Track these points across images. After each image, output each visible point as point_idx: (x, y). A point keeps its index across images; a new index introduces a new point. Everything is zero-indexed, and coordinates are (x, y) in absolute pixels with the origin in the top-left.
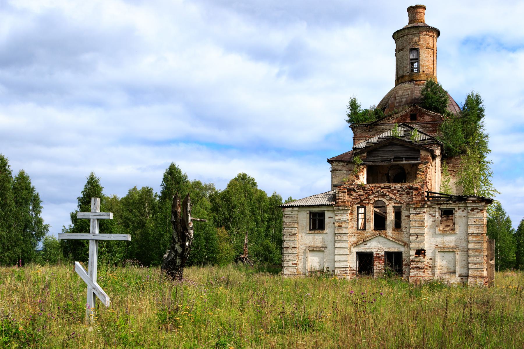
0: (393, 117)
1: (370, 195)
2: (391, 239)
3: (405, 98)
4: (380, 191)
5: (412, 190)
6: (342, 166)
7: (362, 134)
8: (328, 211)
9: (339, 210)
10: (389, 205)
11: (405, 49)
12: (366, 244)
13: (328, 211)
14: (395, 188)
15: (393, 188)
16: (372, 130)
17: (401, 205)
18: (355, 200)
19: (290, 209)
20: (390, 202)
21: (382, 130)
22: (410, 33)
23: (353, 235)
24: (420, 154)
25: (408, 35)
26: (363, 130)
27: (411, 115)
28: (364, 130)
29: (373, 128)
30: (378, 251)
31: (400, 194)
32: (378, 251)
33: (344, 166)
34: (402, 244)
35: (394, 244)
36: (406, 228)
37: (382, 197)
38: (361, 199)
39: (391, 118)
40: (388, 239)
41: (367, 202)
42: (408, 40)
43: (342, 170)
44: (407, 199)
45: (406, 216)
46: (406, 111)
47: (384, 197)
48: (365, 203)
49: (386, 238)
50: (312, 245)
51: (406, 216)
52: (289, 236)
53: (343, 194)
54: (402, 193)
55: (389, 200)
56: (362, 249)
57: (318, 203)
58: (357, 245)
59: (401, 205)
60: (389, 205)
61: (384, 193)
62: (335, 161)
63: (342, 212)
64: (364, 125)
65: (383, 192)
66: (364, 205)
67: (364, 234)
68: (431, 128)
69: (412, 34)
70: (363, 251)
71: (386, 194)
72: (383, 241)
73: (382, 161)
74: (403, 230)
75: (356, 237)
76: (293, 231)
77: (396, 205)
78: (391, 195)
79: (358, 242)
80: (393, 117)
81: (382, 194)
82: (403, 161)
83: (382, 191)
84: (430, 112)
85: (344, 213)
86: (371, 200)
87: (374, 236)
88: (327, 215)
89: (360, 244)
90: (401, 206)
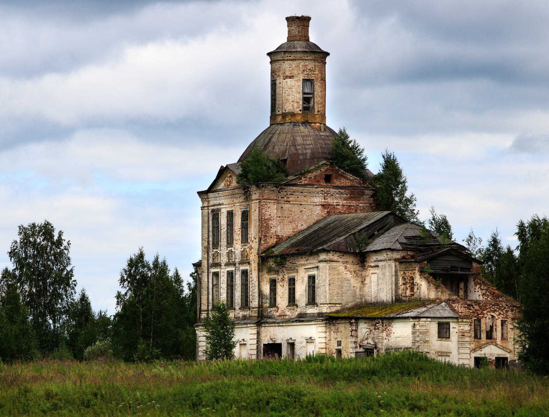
0: (306, 177)
1: (484, 311)
2: (500, 347)
3: (309, 149)
4: (492, 307)
5: (515, 308)
6: (338, 256)
7: (270, 195)
8: (452, 322)
9: (463, 322)
10: (498, 319)
11: (297, 79)
12: (481, 351)
13: (452, 322)
14: (502, 305)
15: (501, 305)
16: (282, 191)
17: (507, 319)
18: (473, 314)
19: (425, 319)
20: (499, 316)
21: (293, 192)
22: (304, 58)
23: (472, 342)
24: (472, 266)
25: (302, 60)
26: (271, 191)
27: (326, 175)
28: (273, 191)
29: (284, 189)
30: (491, 356)
31: (506, 311)
32: (491, 356)
33: (340, 257)
34: (508, 351)
35: (502, 351)
36: (511, 338)
37: (493, 312)
38: (477, 313)
39: (304, 178)
40: (498, 347)
41: (482, 316)
42: (300, 66)
43: (338, 261)
44: (511, 315)
45: (511, 329)
46: (321, 171)
47: (494, 313)
48: (480, 317)
49: (496, 346)
50: (440, 350)
51: (511, 329)
52: (423, 343)
53: (464, 309)
54: (508, 310)
55: (498, 315)
56: (478, 354)
57: (445, 316)
58: (475, 351)
59: (507, 319)
60: (498, 319)
61: (495, 309)
62: (332, 251)
63: (465, 323)
64: (275, 185)
65: (494, 309)
66: (480, 318)
67: (480, 342)
68: (349, 195)
69: (306, 60)
70: (480, 356)
71: (496, 310)
72: (494, 348)
73: (442, 270)
74: (509, 340)
75: (474, 344)
76: (426, 338)
77: (503, 319)
78: (500, 311)
79: (476, 349)
80: (306, 177)
81: (493, 310)
82: (458, 271)
83: (493, 307)
84: (349, 174)
85: (466, 324)
86: (485, 314)
87: (487, 344)
88: (452, 325)
89: (478, 350)
90: (507, 320)
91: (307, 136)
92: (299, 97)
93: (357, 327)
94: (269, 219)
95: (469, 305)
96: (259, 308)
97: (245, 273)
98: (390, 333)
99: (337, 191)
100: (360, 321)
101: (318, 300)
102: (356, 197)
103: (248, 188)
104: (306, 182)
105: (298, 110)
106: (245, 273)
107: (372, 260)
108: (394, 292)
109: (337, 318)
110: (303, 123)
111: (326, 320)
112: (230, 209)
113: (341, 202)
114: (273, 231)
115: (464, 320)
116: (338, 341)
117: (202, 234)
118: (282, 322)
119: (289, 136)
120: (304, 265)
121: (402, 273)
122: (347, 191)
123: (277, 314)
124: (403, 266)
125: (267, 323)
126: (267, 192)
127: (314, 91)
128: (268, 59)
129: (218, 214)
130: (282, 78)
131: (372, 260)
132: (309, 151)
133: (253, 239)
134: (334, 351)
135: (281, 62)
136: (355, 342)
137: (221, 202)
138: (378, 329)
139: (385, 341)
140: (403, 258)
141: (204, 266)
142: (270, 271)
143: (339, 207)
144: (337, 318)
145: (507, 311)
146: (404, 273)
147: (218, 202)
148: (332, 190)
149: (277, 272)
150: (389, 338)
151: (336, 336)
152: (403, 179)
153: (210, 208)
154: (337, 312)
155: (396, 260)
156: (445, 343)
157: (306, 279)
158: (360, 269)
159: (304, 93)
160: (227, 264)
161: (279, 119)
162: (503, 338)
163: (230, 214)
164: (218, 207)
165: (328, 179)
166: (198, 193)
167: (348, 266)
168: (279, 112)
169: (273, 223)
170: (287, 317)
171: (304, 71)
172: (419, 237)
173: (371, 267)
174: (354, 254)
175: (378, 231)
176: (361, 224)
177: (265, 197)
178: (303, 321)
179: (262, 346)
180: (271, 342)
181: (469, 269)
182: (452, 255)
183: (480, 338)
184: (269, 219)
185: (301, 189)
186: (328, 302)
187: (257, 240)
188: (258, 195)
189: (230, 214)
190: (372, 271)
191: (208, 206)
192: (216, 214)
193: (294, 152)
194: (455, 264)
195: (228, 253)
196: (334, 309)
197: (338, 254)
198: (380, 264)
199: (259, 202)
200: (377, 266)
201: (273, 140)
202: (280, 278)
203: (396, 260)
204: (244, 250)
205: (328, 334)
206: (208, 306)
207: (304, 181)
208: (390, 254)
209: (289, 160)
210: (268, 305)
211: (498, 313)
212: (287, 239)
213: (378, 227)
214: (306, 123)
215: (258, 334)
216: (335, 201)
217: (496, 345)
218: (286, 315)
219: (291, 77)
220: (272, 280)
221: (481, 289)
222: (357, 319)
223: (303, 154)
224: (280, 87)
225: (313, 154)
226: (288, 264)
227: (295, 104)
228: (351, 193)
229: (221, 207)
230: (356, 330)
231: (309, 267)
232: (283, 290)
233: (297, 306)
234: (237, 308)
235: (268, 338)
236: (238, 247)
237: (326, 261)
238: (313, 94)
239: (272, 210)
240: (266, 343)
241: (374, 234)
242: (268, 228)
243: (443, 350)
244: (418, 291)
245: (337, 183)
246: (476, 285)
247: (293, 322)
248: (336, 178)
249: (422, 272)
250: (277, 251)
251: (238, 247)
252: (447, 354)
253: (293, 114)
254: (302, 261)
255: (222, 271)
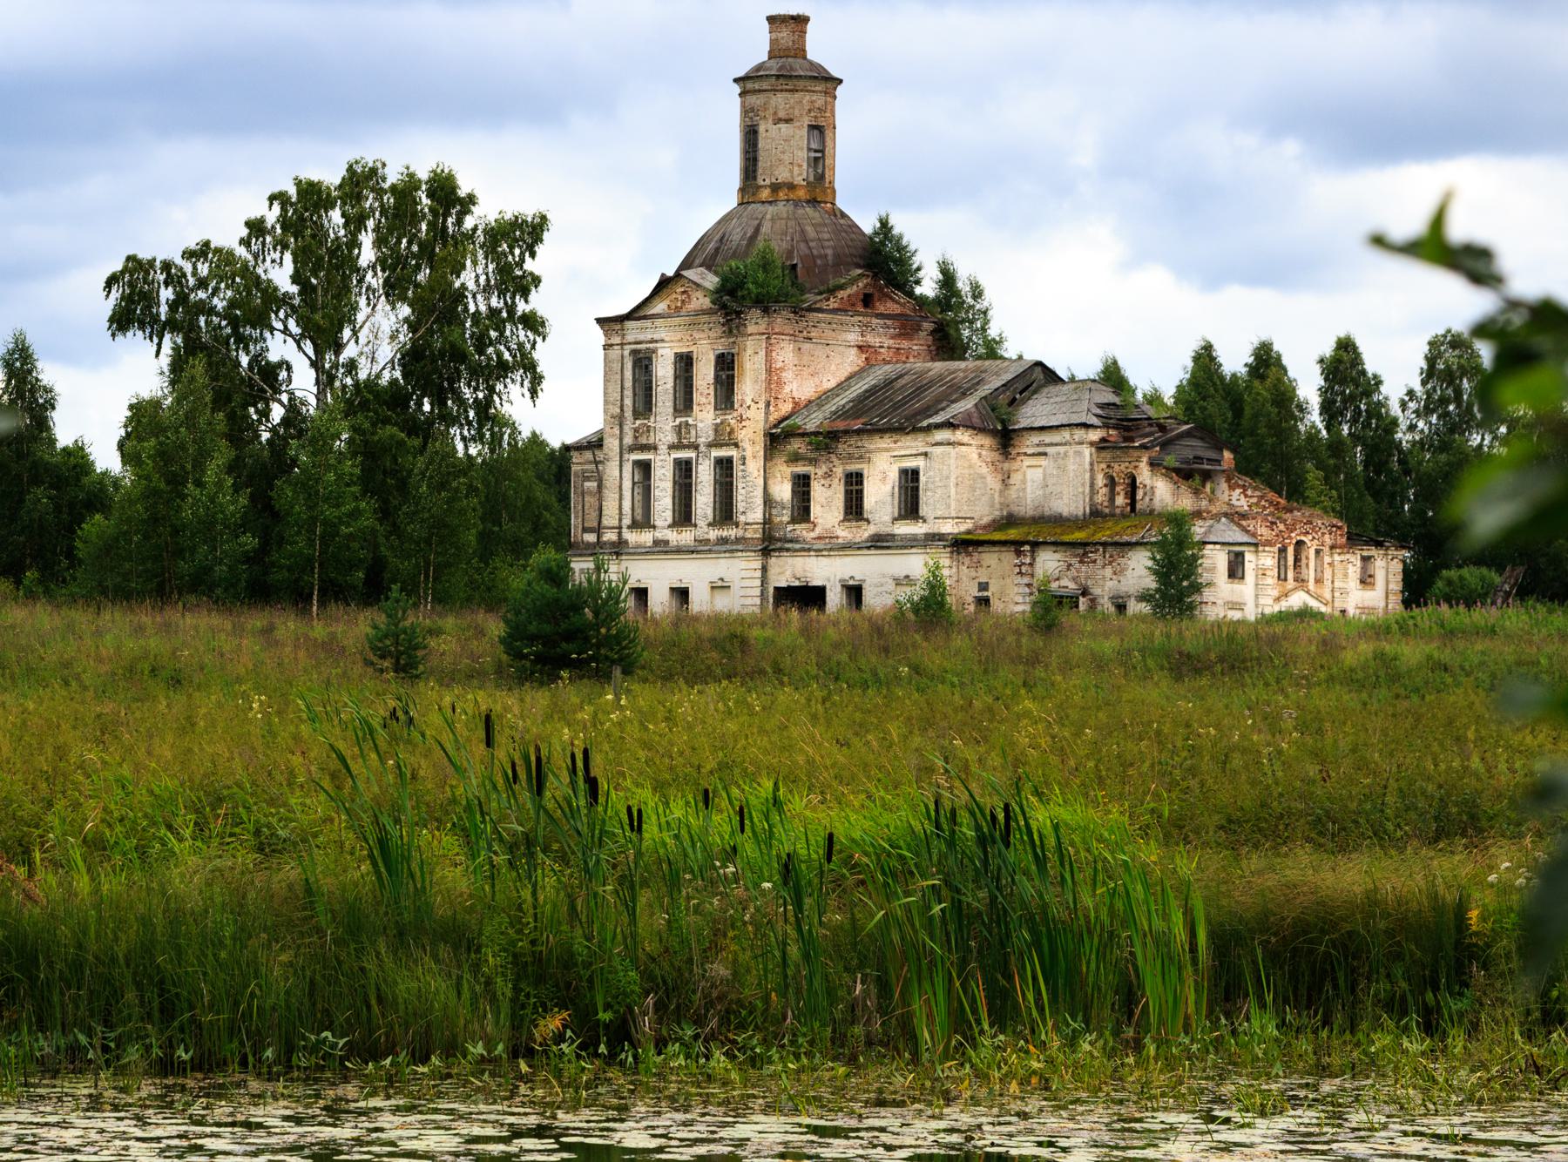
88: (1249, 557)
91: (820, 225)
92: (802, 156)
93: (1034, 559)
94: (781, 369)
95: (1272, 523)
96: (764, 523)
97: (725, 468)
98: (1122, 571)
99: (882, 322)
100: (1042, 547)
101: (924, 510)
102: (908, 334)
103: (738, 313)
104: (836, 306)
105: (800, 178)
106: (725, 468)
107: (1028, 443)
108: (1087, 500)
109: (979, 543)
110: (808, 202)
111: (952, 545)
112: (685, 350)
113: (888, 342)
114: (787, 389)
115: (1267, 549)
116: (980, 584)
117: (605, 394)
118: (831, 550)
119: (792, 223)
120: (887, 450)
121: (1103, 466)
122: (897, 324)
123: (813, 535)
124: (1107, 455)
125: (788, 550)
126: (780, 321)
127: (824, 146)
128: (737, 89)
129: (650, 359)
130: (770, 121)
131: (1030, 443)
132: (829, 252)
133: (749, 402)
134: (970, 599)
135: (770, 94)
136: (1029, 585)
137: (656, 337)
138: (1094, 561)
139: (1109, 584)
140: (1103, 440)
141: (611, 450)
142: (795, 458)
143: (882, 350)
144: (979, 543)
145: (1323, 534)
146: (1109, 467)
147: (649, 337)
148: (875, 321)
149: (813, 462)
150: (1121, 578)
151: (974, 574)
152: (986, 304)
153: (626, 347)
154: (969, 532)
155: (1092, 444)
156: (1237, 586)
157: (894, 475)
158: (1001, 458)
159: (809, 149)
160: (672, 447)
161: (765, 194)
162: (1318, 581)
163: (685, 363)
164: (651, 346)
165: (867, 300)
166: (600, 321)
167: (984, 453)
168: (763, 179)
169: (787, 376)
170: (840, 541)
171: (810, 110)
172: (1114, 404)
173: (1025, 454)
174: (993, 433)
175: (1021, 393)
176: (978, 383)
177: (777, 330)
178: (888, 548)
179: (771, 590)
180: (797, 583)
181: (1218, 462)
182: (1195, 437)
183: (1286, 580)
184: (781, 369)
185: (829, 317)
186: (954, 515)
187: (762, 405)
188: (764, 326)
189: (685, 363)
190: (1028, 461)
191: (622, 344)
192: (643, 362)
193: (807, 252)
194: (1200, 453)
195: (680, 426)
196: (963, 527)
197: (970, 432)
198: (1049, 450)
199: (768, 338)
200: (1045, 454)
201: (763, 230)
202: (820, 472)
203: (1092, 444)
204: (722, 423)
205: (954, 570)
206: (620, 520)
207: (833, 303)
208: (1079, 434)
209: (800, 266)
210: (786, 519)
211: (1310, 537)
212: (806, 406)
213: (1020, 386)
214: (813, 202)
215: (764, 569)
216: (877, 340)
217: (1308, 592)
218: (837, 537)
219: (788, 121)
220: (799, 476)
221: (1246, 496)
222: (1035, 545)
223: (820, 256)
224: (766, 138)
225: (837, 256)
226: (842, 448)
227: (796, 168)
228: (903, 327)
229: (658, 345)
230: (1031, 564)
231: (903, 453)
232: (829, 493)
233: (868, 521)
234: (702, 523)
235: (788, 573)
236: (705, 417)
237: (949, 444)
238: (822, 151)
239: (785, 354)
240: (783, 584)
241: (1014, 399)
242: (780, 383)
243: (1235, 600)
244: (1147, 499)
245: (881, 308)
246: (1232, 488)
247: (859, 548)
248: (879, 300)
249: (1153, 464)
250: (813, 421)
251: (705, 417)
252: (1238, 606)
253: (791, 187)
254: (884, 442)
255: (658, 458)
